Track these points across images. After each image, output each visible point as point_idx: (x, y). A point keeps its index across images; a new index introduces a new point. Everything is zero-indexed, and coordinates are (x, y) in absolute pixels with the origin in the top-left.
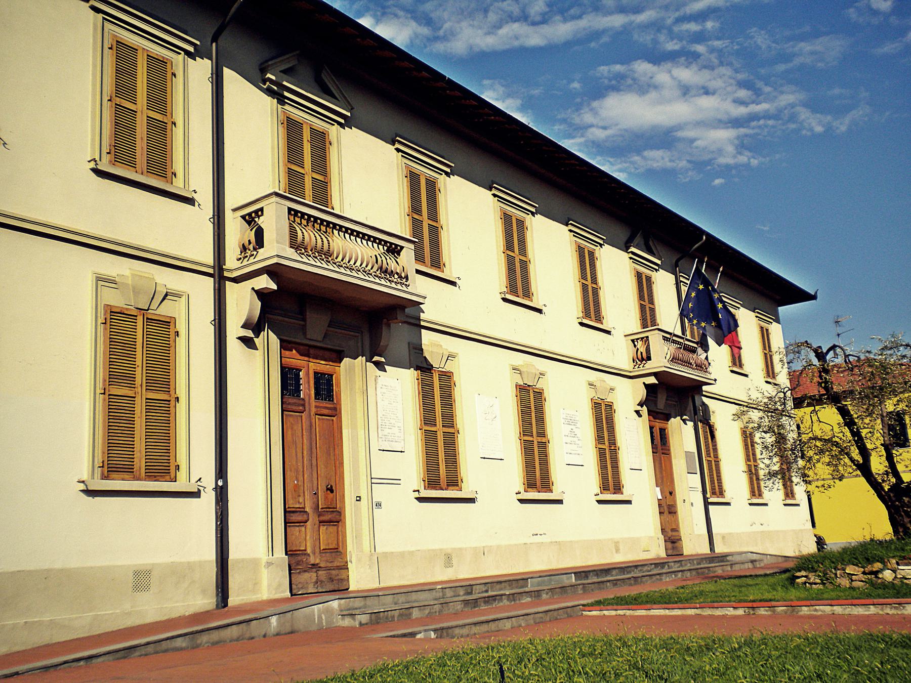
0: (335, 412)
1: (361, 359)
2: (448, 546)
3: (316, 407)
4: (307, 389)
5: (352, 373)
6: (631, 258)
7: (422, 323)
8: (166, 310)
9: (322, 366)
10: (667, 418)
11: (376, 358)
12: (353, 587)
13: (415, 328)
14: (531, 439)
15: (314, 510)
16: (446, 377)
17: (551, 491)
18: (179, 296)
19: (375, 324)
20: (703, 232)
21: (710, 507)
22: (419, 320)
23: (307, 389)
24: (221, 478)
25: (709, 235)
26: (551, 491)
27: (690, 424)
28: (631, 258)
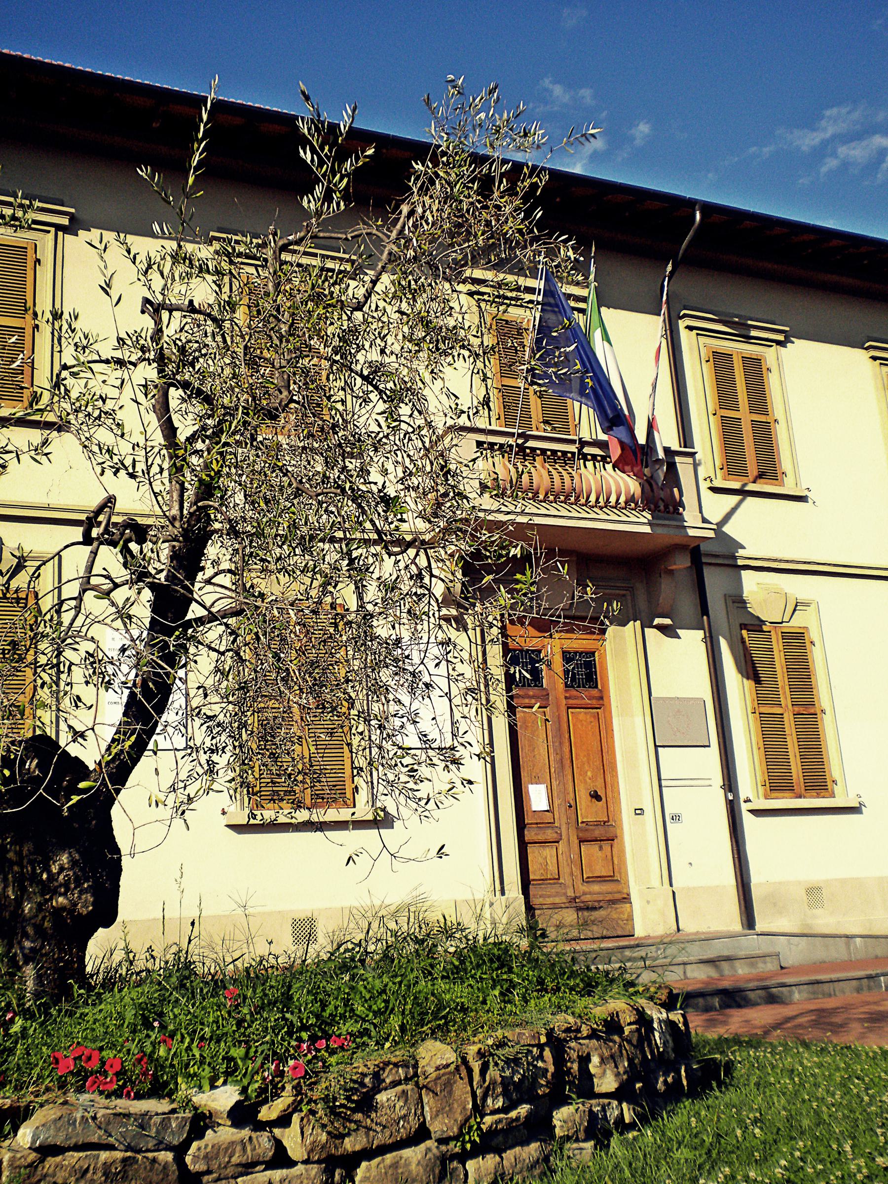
0: (600, 702)
1: (633, 627)
2: (816, 876)
3: (566, 698)
4: (554, 676)
5: (619, 647)
6: (874, 358)
7: (740, 562)
8: (797, 622)
9: (578, 642)
10: (596, 626)
11: (657, 621)
12: (640, 931)
13: (730, 571)
14: (778, 710)
15: (565, 837)
16: (797, 640)
17: (833, 795)
18: (807, 605)
19: (664, 572)
20: (691, 204)
21: (530, 849)
22: (735, 558)
23: (554, 676)
24: (731, 801)
25: (709, 209)
26: (833, 795)
27: (692, 640)
28: (874, 358)
